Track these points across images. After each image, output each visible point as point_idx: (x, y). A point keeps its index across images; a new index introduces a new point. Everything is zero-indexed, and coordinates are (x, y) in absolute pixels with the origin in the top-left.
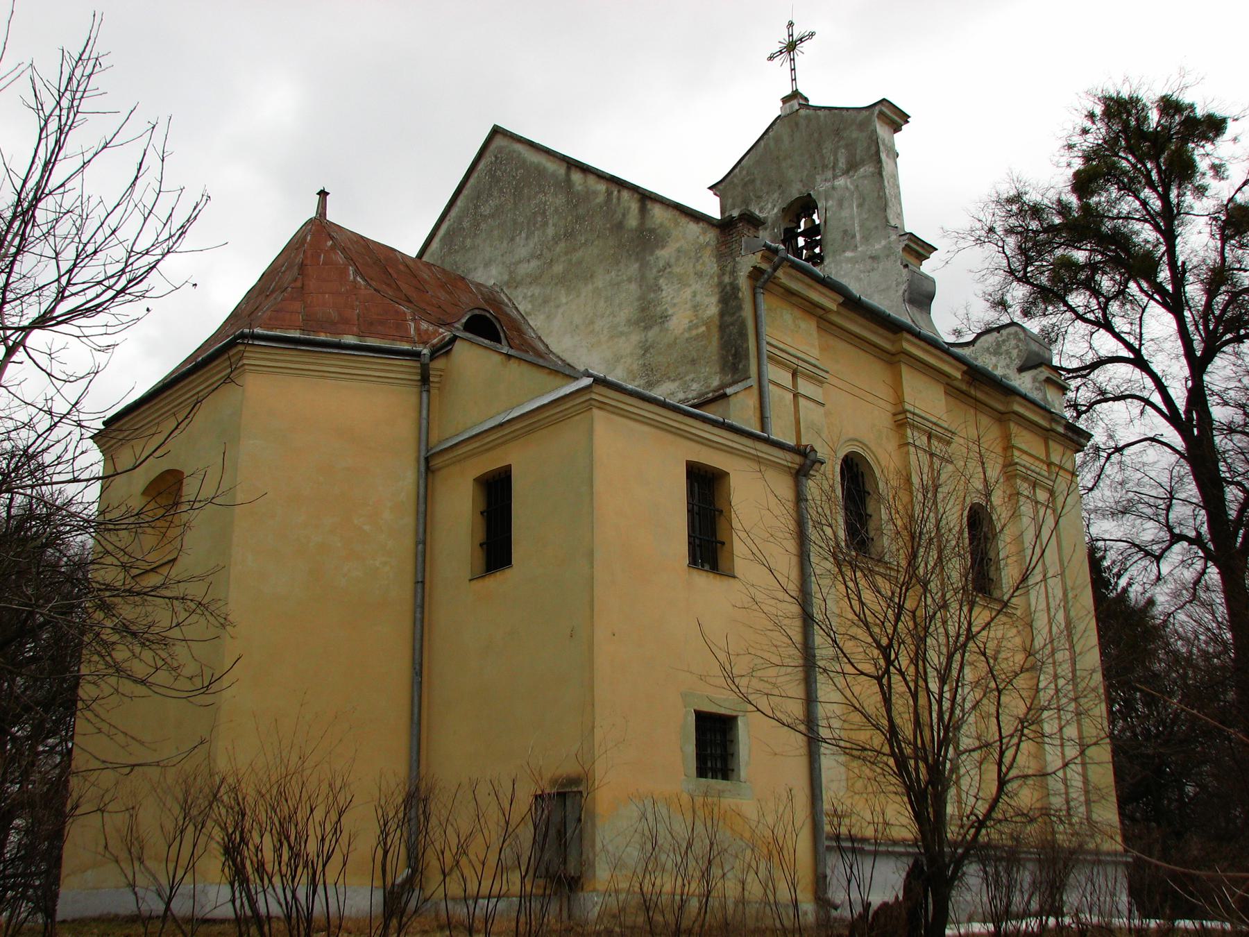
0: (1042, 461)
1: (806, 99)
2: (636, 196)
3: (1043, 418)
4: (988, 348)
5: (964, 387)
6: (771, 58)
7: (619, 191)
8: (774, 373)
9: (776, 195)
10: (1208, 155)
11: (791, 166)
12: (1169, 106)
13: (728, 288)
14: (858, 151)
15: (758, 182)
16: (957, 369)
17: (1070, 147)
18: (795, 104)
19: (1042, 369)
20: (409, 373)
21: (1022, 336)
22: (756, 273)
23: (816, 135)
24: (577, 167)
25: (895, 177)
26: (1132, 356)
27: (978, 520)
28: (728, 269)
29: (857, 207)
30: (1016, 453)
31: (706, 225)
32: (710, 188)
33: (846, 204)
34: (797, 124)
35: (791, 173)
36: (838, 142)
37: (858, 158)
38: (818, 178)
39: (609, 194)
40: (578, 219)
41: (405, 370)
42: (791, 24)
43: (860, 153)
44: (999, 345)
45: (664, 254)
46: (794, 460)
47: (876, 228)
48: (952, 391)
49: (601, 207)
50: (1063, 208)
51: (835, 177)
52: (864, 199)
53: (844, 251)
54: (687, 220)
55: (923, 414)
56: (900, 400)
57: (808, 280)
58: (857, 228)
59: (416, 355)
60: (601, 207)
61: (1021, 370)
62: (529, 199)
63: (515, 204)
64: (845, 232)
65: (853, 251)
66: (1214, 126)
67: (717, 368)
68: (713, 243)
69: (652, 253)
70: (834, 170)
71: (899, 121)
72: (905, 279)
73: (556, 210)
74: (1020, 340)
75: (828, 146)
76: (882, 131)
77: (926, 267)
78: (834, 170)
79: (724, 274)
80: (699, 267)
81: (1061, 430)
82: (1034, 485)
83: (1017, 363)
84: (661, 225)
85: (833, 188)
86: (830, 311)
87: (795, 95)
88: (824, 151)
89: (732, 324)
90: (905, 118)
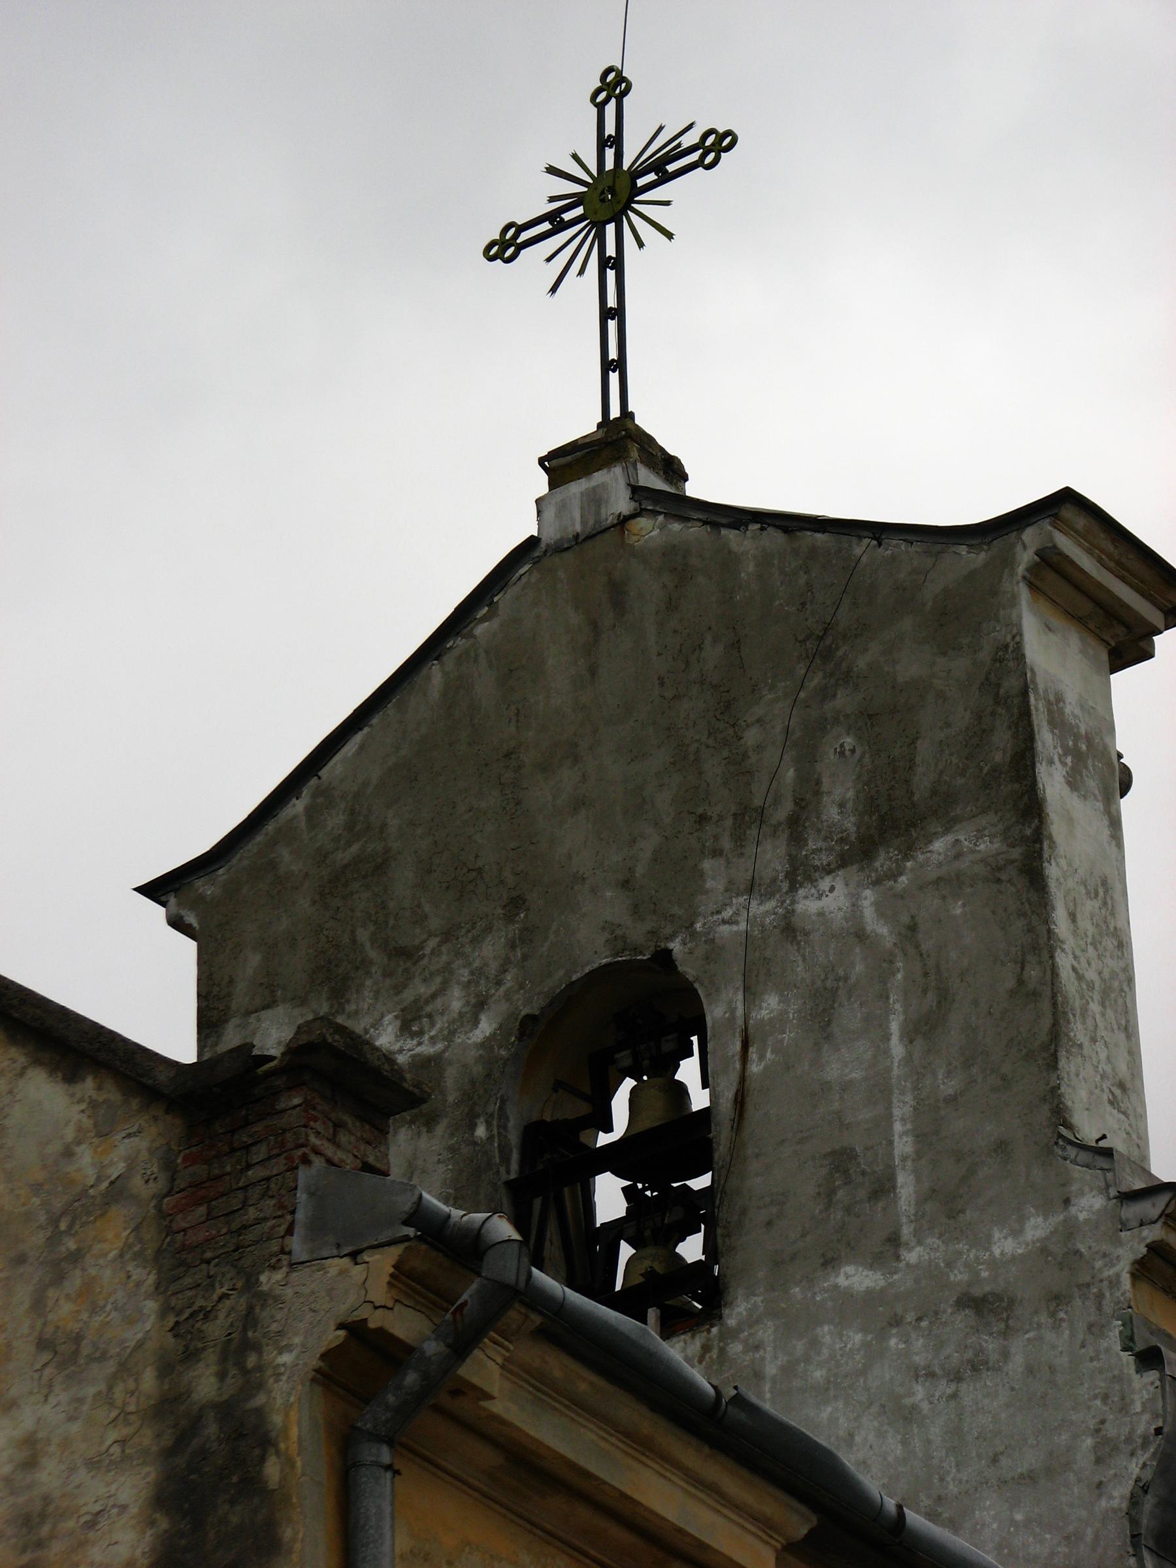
1: (673, 469)
9: (490, 950)
11: (578, 804)
13: (211, 1429)
14: (924, 749)
15: (403, 878)
23: (713, 654)
28: (216, 1329)
29: (909, 1037)
31: (112, 1094)
32: (153, 890)
33: (850, 1016)
34: (617, 592)
36: (825, 694)
37: (923, 781)
47: (1002, 1147)
52: (944, 996)
53: (830, 1262)
58: (903, 1145)
65: (876, 1261)
70: (797, 839)
72: (1144, 1425)
78: (797, 839)
79: (190, 1356)
85: (790, 929)
88: (752, 736)
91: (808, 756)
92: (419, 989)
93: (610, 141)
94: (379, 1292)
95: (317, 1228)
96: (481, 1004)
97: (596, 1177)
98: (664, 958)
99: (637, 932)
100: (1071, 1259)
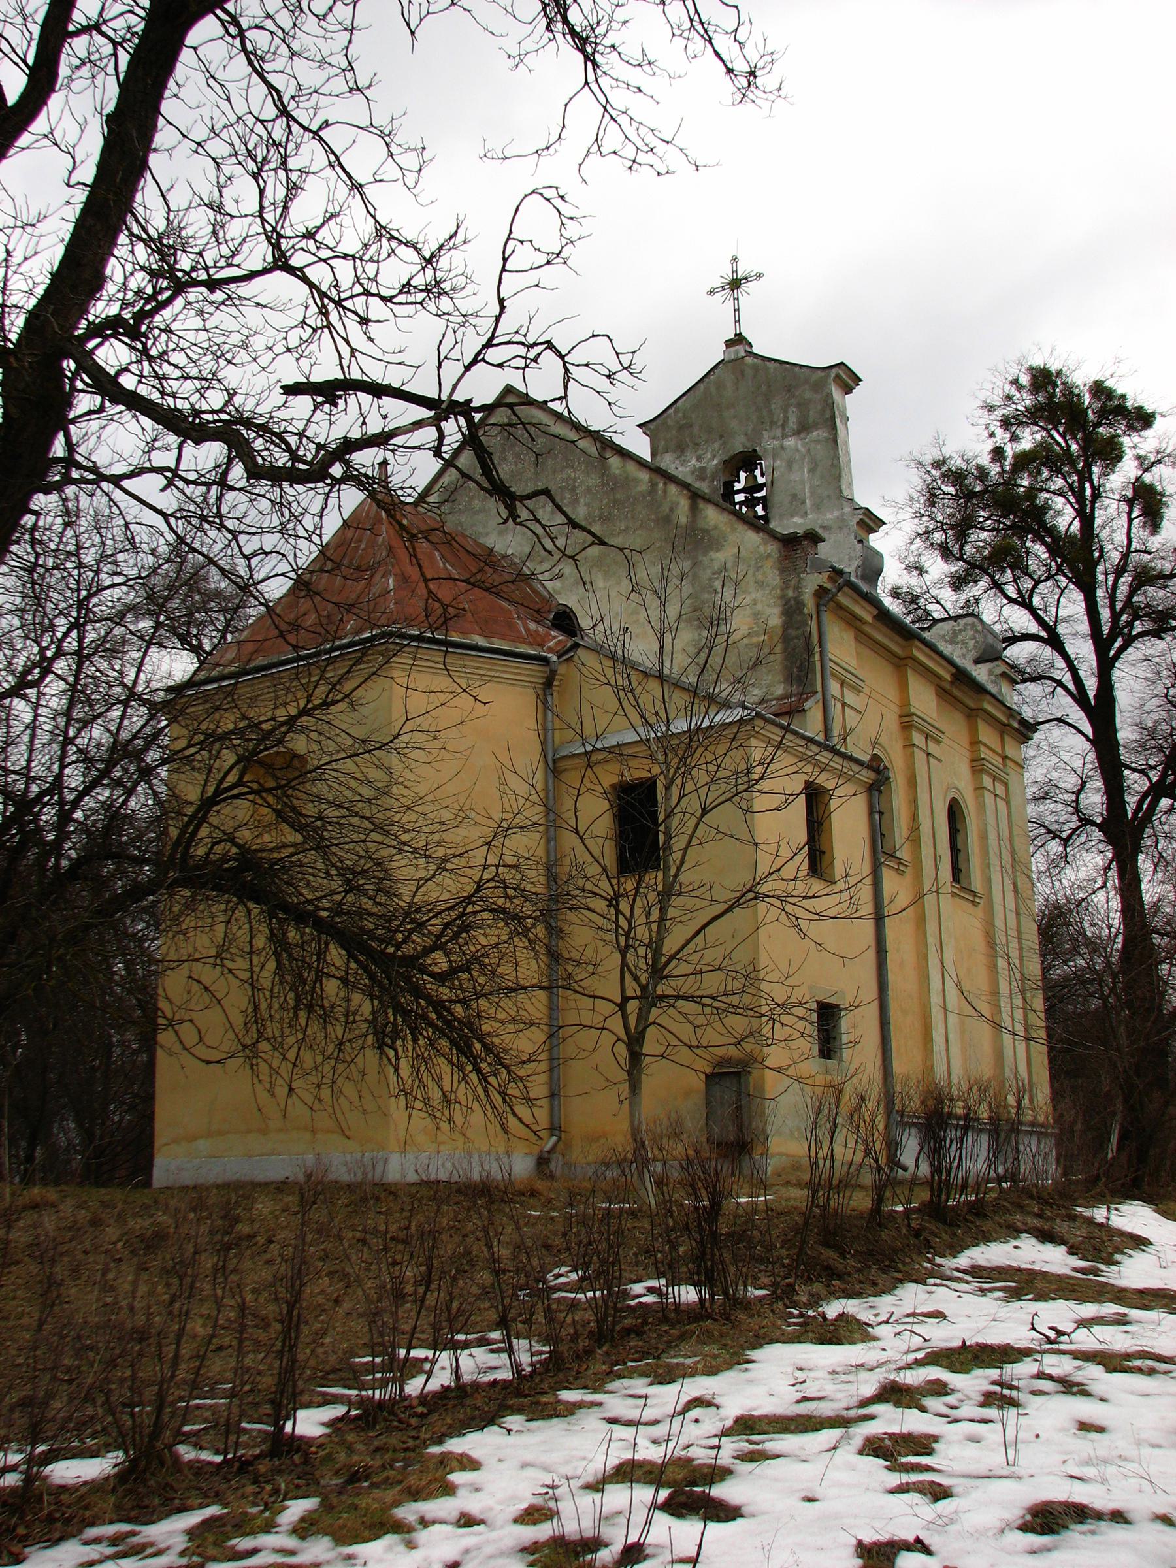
0: (997, 754)
1: (750, 345)
2: (685, 492)
3: (1004, 713)
4: (944, 636)
5: (947, 686)
6: (711, 292)
7: (665, 484)
8: (834, 688)
9: (716, 445)
10: (752, 73)
11: (735, 417)
12: (1099, 389)
13: (792, 602)
14: (811, 413)
15: (696, 430)
16: (949, 672)
17: (991, 408)
18: (741, 350)
19: (999, 663)
20: (538, 677)
21: (980, 628)
22: (821, 592)
23: (764, 388)
24: (612, 449)
25: (846, 443)
26: (1043, 634)
27: (955, 812)
28: (793, 583)
29: (809, 472)
30: (982, 748)
31: (766, 537)
32: (639, 426)
33: (795, 467)
34: (742, 373)
35: (734, 424)
36: (789, 399)
37: (811, 420)
38: (765, 435)
39: (653, 485)
40: (616, 502)
41: (532, 672)
42: (735, 259)
43: (812, 416)
44: (955, 634)
45: (719, 557)
46: (867, 776)
47: (828, 496)
48: (943, 694)
49: (644, 497)
50: (983, 473)
51: (784, 436)
52: (816, 465)
53: (792, 516)
54: (746, 527)
55: (922, 715)
56: (905, 702)
57: (855, 596)
58: (807, 494)
59: (546, 661)
60: (644, 497)
61: (977, 662)
62: (554, 472)
63: (536, 473)
64: (794, 496)
65: (802, 517)
66: (1142, 419)
67: (780, 678)
68: (776, 555)
69: (705, 553)
70: (784, 429)
71: (853, 385)
72: (859, 554)
73: (588, 489)
74: (977, 631)
75: (777, 404)
76: (836, 394)
77: (876, 541)
78: (784, 429)
79: (787, 588)
80: (759, 576)
81: (1016, 725)
82: (994, 779)
83: (974, 654)
84: (716, 527)
85: (782, 447)
86: (866, 623)
87: (739, 339)
88: (773, 406)
89: (797, 637)
90: (857, 380)
91: (785, 411)
92: (700, 452)
93: (734, 272)
94: (825, 580)
95: (811, 567)
96: (714, 457)
97: (25, 79)
98: (755, 451)
99: (749, 445)
100: (843, 520)
